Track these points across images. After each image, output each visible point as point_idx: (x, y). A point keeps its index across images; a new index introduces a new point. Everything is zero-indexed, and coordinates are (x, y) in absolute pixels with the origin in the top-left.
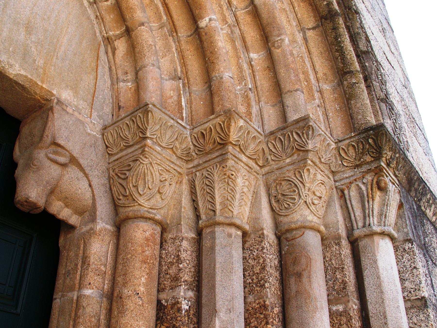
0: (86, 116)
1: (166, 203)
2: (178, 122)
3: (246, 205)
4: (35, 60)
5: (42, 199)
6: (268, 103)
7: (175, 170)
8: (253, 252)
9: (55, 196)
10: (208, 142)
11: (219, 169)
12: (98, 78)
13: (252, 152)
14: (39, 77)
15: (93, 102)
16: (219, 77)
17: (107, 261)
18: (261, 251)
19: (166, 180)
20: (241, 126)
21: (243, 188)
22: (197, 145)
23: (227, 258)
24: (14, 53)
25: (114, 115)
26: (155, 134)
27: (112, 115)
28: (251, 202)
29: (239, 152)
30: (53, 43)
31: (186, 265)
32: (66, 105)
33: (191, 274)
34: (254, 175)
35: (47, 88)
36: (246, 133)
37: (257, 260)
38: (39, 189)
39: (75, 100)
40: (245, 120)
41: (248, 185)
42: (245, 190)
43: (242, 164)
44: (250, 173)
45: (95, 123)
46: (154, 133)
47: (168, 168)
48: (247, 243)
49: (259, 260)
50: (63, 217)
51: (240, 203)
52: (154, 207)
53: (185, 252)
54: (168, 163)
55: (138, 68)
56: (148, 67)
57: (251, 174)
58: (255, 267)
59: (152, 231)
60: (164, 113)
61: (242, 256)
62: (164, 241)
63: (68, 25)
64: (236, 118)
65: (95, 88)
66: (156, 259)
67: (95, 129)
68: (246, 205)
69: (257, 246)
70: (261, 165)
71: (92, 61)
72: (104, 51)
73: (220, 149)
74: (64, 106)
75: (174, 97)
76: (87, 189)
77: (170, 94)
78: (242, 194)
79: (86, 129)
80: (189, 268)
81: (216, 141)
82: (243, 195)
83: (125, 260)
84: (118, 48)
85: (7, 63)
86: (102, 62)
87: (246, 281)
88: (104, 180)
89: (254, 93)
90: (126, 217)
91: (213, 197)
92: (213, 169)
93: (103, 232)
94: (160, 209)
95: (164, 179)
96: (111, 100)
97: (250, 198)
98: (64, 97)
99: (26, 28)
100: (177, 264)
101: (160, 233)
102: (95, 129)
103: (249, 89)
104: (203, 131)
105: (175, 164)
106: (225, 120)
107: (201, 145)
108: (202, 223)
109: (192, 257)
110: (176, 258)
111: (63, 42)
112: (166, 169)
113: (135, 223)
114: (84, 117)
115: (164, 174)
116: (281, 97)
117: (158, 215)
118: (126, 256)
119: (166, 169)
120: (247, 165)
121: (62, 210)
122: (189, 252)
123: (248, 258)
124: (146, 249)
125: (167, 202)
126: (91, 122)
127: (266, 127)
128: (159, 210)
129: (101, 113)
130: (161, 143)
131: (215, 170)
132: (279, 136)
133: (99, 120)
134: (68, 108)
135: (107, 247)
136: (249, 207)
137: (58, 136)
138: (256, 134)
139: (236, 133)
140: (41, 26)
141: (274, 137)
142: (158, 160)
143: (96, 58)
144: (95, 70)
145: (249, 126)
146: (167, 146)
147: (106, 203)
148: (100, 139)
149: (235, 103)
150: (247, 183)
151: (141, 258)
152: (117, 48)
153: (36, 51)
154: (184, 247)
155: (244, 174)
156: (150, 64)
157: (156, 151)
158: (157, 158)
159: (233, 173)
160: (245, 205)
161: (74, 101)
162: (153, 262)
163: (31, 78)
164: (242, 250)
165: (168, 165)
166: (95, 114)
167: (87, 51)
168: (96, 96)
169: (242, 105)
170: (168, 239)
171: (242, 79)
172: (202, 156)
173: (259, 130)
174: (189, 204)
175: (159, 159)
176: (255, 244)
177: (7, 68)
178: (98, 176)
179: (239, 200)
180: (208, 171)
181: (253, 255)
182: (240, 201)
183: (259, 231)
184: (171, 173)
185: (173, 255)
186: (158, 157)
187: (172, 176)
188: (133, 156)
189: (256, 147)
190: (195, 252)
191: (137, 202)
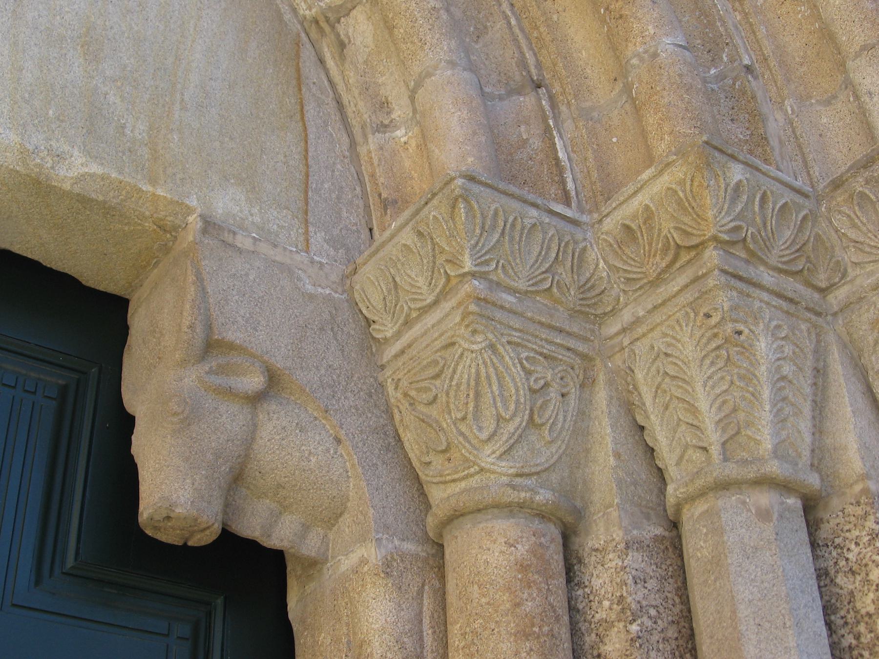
0: (294, 249)
1: (561, 451)
2: (551, 212)
3: (798, 413)
4: (123, 127)
5: (209, 503)
6: (811, 97)
7: (569, 349)
8: (845, 551)
9: (248, 488)
10: (650, 251)
11: (695, 321)
12: (311, 136)
13: (788, 252)
14: (143, 170)
15: (307, 204)
16: (646, 56)
17: (422, 647)
18: (869, 545)
19: (546, 385)
20: (739, 184)
21: (779, 368)
22: (620, 265)
23: (766, 584)
24: (62, 121)
25: (375, 228)
26: (491, 260)
27: (367, 231)
28: (814, 401)
29: (747, 262)
30: (165, 70)
31: (649, 623)
32: (229, 231)
33: (669, 648)
34: (808, 320)
35: (169, 196)
36: (757, 199)
37: (863, 574)
38: (197, 477)
39: (255, 210)
40: (746, 164)
41: (794, 353)
42: (787, 369)
43: (765, 296)
44: (792, 315)
45: (324, 261)
46: (487, 257)
47: (547, 349)
48: (822, 526)
49: (867, 575)
50: (282, 540)
51: (779, 410)
52: (526, 470)
53: (639, 586)
54: (544, 334)
55: (413, 83)
56: (438, 72)
57: (798, 317)
58: (858, 597)
59: (534, 538)
60: (504, 193)
61: (813, 570)
62: (575, 561)
63: (199, 9)
64: (719, 162)
65: (307, 165)
66: (557, 619)
67: (327, 278)
68: (798, 413)
69: (853, 531)
70: (823, 285)
71: (284, 93)
72: (314, 58)
73: (689, 262)
74: (226, 235)
75: (531, 141)
76: (332, 452)
77: (520, 135)
78: (778, 385)
79: (300, 285)
80: (659, 629)
81: (672, 243)
82: (784, 388)
83: (469, 638)
84: (350, 41)
85: (46, 153)
86: (314, 89)
87: (839, 643)
88: (377, 417)
89: (763, 76)
90: (452, 512)
91: (693, 410)
92: (677, 328)
93: (395, 564)
94: (546, 470)
95: (542, 382)
96: (358, 189)
97: (808, 390)
98: (220, 211)
99: (82, 46)
100: (621, 625)
101: (560, 540)
102: (327, 278)
103: (744, 70)
104: (627, 222)
105: (569, 334)
106: (685, 174)
107: (633, 263)
108: (675, 490)
109: (663, 596)
110: (615, 606)
111: (193, 61)
112: (541, 354)
113: (481, 525)
114: (287, 253)
115: (539, 369)
116: (845, 71)
117: (542, 491)
118: (468, 625)
119: (541, 354)
120: (779, 295)
121: (275, 521)
122: (652, 584)
123: (832, 572)
124: (525, 596)
125: (564, 447)
126: (312, 262)
127: (816, 169)
128: (544, 476)
129: (336, 232)
130: (425, 303)
131: (685, 328)
132: (861, 189)
133: (332, 252)
134: (239, 237)
135: (415, 604)
136: (809, 417)
137: (221, 320)
138: (788, 197)
139: (726, 207)
140: (123, 33)
141: (847, 195)
142: (514, 333)
143: (294, 82)
144: (298, 117)
145: (762, 179)
146: (533, 285)
147: (393, 479)
148: (346, 304)
149: (710, 120)
150: (788, 350)
151: (512, 625)
152: (346, 41)
153: (122, 101)
154: (634, 572)
155: (774, 323)
156: (443, 63)
157: (502, 307)
158: (511, 327)
159: (741, 327)
160: (795, 414)
161: (252, 215)
162: (552, 630)
163: (121, 178)
164: (809, 550)
165: (546, 340)
166: (318, 238)
167: (265, 69)
168: (314, 186)
169: (732, 120)
170: (585, 555)
171: (718, 45)
172: (640, 296)
173: (798, 184)
174: (631, 440)
175: (516, 330)
176: (847, 527)
177: (49, 165)
178: (357, 409)
179: (775, 405)
180: (665, 335)
181: (847, 559)
182: (779, 405)
183: (851, 485)
184: (561, 360)
185: (608, 599)
186: (511, 323)
187: (566, 370)
188: (442, 335)
189: (797, 234)
190: (670, 580)
191: (475, 463)
